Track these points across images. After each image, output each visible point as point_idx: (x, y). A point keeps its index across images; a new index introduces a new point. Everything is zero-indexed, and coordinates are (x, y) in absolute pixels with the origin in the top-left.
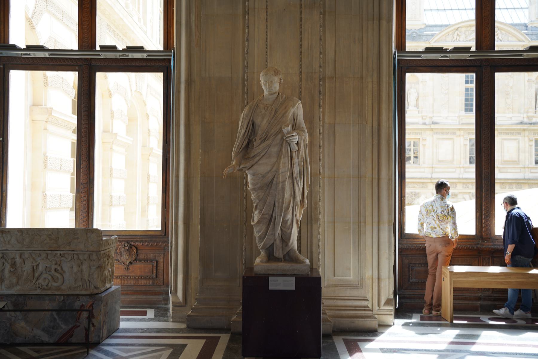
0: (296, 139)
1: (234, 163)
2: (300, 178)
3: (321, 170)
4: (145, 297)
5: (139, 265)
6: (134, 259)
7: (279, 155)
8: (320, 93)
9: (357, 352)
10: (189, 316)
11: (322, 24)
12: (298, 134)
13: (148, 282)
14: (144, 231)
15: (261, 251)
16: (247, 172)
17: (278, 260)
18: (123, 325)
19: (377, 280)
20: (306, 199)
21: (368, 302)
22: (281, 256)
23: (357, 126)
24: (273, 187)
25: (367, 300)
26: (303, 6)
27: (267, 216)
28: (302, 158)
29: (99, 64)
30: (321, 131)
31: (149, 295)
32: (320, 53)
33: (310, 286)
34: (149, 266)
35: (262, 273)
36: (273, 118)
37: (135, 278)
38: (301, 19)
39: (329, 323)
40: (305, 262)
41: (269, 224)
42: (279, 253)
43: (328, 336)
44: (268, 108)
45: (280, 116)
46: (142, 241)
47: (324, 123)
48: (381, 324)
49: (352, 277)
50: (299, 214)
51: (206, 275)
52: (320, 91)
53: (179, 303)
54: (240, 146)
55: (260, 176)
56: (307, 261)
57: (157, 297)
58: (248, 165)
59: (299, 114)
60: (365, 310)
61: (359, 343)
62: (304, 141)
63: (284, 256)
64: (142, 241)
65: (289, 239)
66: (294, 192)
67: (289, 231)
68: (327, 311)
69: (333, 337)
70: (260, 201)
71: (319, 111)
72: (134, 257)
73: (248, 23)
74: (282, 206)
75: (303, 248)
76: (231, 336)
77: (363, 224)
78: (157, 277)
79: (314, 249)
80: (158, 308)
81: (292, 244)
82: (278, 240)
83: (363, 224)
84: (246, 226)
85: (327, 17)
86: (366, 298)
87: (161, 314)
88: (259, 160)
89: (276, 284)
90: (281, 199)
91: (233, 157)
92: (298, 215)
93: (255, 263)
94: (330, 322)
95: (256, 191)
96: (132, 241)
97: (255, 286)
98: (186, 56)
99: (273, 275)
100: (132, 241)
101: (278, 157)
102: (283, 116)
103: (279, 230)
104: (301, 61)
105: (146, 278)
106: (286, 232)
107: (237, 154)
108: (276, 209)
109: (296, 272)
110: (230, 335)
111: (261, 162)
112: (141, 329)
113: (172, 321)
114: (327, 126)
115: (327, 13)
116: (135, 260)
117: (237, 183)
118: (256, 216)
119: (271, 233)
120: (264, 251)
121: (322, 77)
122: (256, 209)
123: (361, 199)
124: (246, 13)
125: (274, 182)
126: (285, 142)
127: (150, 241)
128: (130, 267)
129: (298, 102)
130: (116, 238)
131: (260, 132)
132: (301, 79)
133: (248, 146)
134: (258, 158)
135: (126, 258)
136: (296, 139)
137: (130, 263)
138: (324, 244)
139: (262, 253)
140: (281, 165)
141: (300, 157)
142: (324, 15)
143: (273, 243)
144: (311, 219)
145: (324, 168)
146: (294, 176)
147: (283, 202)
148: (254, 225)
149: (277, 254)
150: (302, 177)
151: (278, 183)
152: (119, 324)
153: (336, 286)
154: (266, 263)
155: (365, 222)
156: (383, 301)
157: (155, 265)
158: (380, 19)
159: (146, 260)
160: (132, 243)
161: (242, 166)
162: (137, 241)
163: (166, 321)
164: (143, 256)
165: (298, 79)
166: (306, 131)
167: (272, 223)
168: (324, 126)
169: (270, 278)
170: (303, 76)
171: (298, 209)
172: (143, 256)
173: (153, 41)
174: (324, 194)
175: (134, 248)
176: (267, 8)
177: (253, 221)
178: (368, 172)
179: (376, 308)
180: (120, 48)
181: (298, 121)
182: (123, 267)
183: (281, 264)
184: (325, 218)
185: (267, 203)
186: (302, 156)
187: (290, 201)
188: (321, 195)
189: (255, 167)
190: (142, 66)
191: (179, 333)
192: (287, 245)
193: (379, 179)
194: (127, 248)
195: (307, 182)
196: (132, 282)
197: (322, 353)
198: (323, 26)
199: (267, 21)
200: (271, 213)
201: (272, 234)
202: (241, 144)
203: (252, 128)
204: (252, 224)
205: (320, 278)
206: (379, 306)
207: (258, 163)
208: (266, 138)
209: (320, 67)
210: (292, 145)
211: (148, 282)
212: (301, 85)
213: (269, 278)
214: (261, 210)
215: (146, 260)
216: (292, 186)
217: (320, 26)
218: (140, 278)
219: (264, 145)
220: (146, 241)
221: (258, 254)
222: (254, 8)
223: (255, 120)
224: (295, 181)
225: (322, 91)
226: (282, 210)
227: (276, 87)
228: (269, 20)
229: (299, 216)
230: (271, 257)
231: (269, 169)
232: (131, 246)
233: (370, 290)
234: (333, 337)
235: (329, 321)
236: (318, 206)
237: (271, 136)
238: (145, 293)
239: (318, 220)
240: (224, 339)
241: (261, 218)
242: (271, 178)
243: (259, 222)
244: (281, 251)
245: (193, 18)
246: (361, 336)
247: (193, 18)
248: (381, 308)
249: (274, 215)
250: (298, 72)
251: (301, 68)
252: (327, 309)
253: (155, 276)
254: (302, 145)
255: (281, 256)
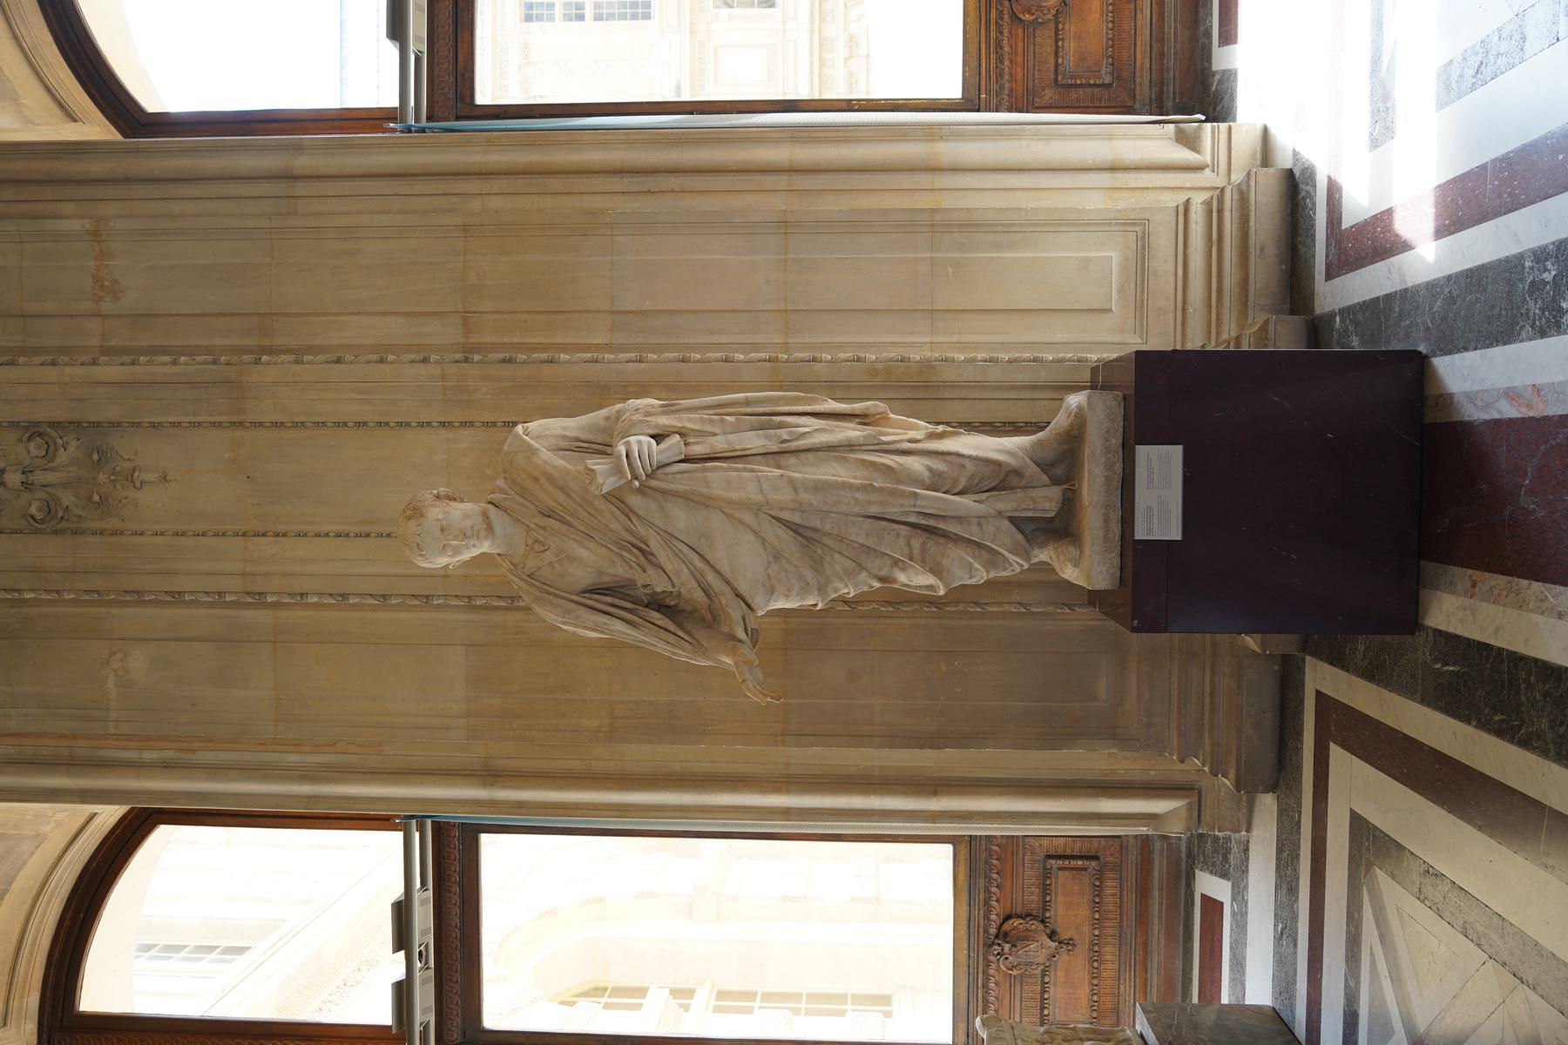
0: (641, 442)
1: (728, 660)
2: (780, 426)
3: (762, 355)
4: (1156, 894)
5: (1060, 912)
6: (1041, 927)
7: (698, 501)
8: (510, 361)
9: (1391, 224)
10: (1238, 786)
11: (293, 357)
12: (625, 434)
13: (1109, 883)
14: (955, 895)
15: (1035, 560)
16: (760, 613)
17: (1070, 504)
18: (1259, 991)
19: (1119, 175)
20: (858, 407)
21: (1193, 202)
22: (1055, 492)
23: (621, 239)
24: (815, 522)
25: (1187, 203)
26: (234, 419)
27: (916, 544)
28: (711, 421)
29: (459, 1020)
30: (632, 355)
31: (1156, 896)
32: (381, 361)
33: (1161, 392)
34: (1062, 880)
35: (1117, 561)
36: (568, 524)
37: (1098, 923)
38: (275, 425)
39: (1271, 327)
40: (1080, 408)
41: (945, 535)
42: (1046, 500)
43: (1316, 329)
44: (536, 541)
45: (562, 498)
46: (987, 903)
47: (609, 347)
48: (1259, 156)
49: (1112, 254)
50: (910, 429)
51: (1109, 731)
52: (504, 361)
53: (1190, 807)
54: (671, 638)
55: (775, 567)
56: (1075, 400)
57: (1156, 856)
58: (735, 611)
59: (559, 431)
60: (1220, 211)
61: (1345, 225)
62: (649, 414)
63: (1055, 481)
64: (987, 903)
65: (998, 464)
66: (831, 448)
67: (970, 466)
68: (1225, 336)
69: (1318, 311)
70: (861, 567)
71: (567, 362)
72: (1035, 925)
73: (291, 595)
74: (881, 490)
75: (1020, 413)
76: (1315, 654)
77: (938, 217)
78: (1096, 858)
79: (1023, 377)
80: (1190, 854)
81: (1008, 452)
82: (1000, 506)
83: (938, 217)
84: (945, 604)
85: (279, 341)
86: (1181, 209)
87: (1229, 864)
88: (719, 573)
89: (1161, 513)
90: (858, 495)
91: (709, 663)
92: (912, 434)
93: (1081, 582)
94: (1266, 322)
95: (828, 582)
96: (986, 931)
97: (1156, 589)
98: (409, 784)
99: (1127, 520)
100: (986, 931)
101: (708, 506)
102: (562, 489)
103: (966, 502)
104: (408, 424)
105: (1098, 891)
106: (971, 477)
107: (698, 648)
108: (893, 511)
109: (1116, 442)
110: (1308, 658)
111: (724, 566)
112: (1278, 939)
113: (1248, 830)
114: (618, 339)
115: (266, 342)
116: (1042, 922)
117: (801, 635)
118: (917, 579)
119: (974, 529)
120: (1036, 551)
121: (458, 356)
122: (895, 581)
123: (859, 224)
124: (257, 599)
125: (796, 518)
126: (653, 483)
127: (987, 877)
128: (1064, 935)
129: (517, 436)
130: (984, 1023)
131: (619, 571)
132: (464, 424)
133: (668, 608)
134: (712, 578)
135: (1039, 949)
136: (641, 442)
137: (1052, 935)
138: (1005, 346)
139: (1043, 555)
140: (735, 496)
141: (709, 428)
142: (270, 351)
143: (1012, 520)
144: (920, 388)
145: (755, 347)
146: (775, 448)
147: (865, 488)
148: (945, 585)
149: (1047, 505)
150: (778, 419)
151: (800, 508)
152: (1257, 1010)
153: (1140, 307)
154: (1080, 547)
155: (933, 210)
156: (1184, 155)
157: (1060, 862)
158: (290, 177)
159: (1045, 890)
160: (993, 931)
161: (741, 634)
162: (987, 918)
163: (1246, 850)
164: (1033, 898)
165: (465, 432)
166: (618, 406)
167: (942, 525)
168: (622, 348)
169: (1140, 535)
170: (455, 416)
171: (890, 436)
172: (1033, 898)
173: (374, 865)
174: (840, 346)
175: (1007, 926)
176: (244, 535)
177: (931, 587)
178: (772, 203)
179: (1207, 178)
180: (399, 973)
181: (583, 437)
182: (1064, 958)
183: (1085, 492)
184: (919, 344)
185: (870, 543)
186: (703, 421)
187: (863, 461)
188: (842, 356)
189: (743, 589)
190: (462, 896)
191: (1298, 823)
192: (1017, 472)
193: (793, 170)
194: (1007, 947)
195: (797, 401)
196: (1111, 931)
197: (1397, 345)
198: (298, 354)
199: (285, 535)
200: (904, 530)
201: (980, 524)
202: (663, 634)
203: (608, 595)
204: (942, 592)
205: (1138, 353)
206: (1199, 168)
207: (728, 574)
208: (640, 550)
209: (425, 361)
210: (664, 459)
211: (1109, 883)
212: (486, 424)
213: (1138, 537)
214: (896, 563)
215: (1045, 890)
216: (810, 455)
217: (297, 362)
218: (1097, 906)
219: (663, 557)
220: (987, 890)
221: (1046, 567)
222: (244, 574)
223: (580, 587)
224: (793, 445)
225: (502, 356)
226: (893, 492)
227: (462, 512)
228: (281, 528)
229: (914, 430)
230: (1060, 528)
231: (751, 537)
232: (1003, 935)
233: (1151, 196)
234: (1318, 311)
235: (1264, 328)
236: (878, 365)
237: (631, 532)
238: (1143, 891)
239: (927, 365)
240: (1321, 677)
241: (923, 562)
242: (780, 531)
243: (936, 571)
244: (1039, 493)
245: (293, 758)
246: (1311, 221)
247: (293, 758)
248: (1209, 161)
249: (913, 519)
250: (444, 433)
251: (429, 424)
252: (1218, 333)
253: (1094, 863)
254: (664, 420)
255: (1055, 492)
